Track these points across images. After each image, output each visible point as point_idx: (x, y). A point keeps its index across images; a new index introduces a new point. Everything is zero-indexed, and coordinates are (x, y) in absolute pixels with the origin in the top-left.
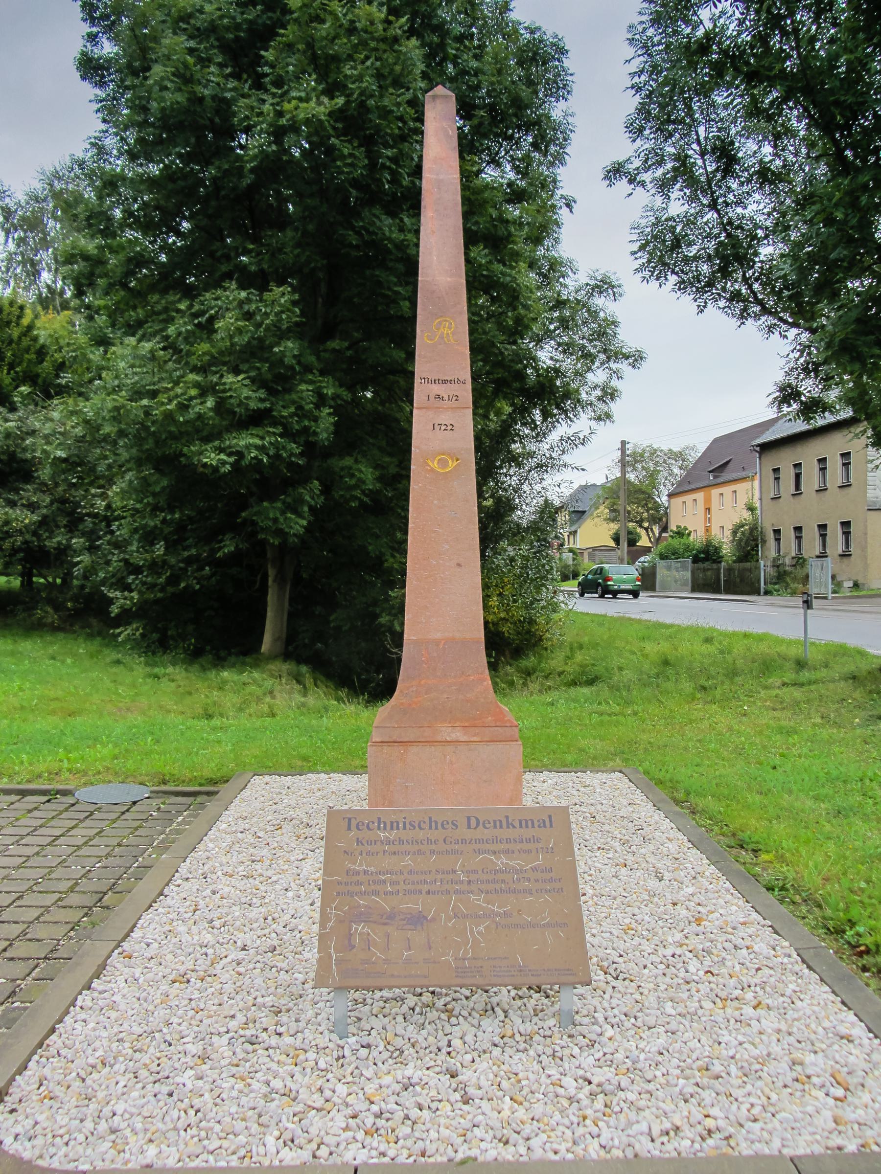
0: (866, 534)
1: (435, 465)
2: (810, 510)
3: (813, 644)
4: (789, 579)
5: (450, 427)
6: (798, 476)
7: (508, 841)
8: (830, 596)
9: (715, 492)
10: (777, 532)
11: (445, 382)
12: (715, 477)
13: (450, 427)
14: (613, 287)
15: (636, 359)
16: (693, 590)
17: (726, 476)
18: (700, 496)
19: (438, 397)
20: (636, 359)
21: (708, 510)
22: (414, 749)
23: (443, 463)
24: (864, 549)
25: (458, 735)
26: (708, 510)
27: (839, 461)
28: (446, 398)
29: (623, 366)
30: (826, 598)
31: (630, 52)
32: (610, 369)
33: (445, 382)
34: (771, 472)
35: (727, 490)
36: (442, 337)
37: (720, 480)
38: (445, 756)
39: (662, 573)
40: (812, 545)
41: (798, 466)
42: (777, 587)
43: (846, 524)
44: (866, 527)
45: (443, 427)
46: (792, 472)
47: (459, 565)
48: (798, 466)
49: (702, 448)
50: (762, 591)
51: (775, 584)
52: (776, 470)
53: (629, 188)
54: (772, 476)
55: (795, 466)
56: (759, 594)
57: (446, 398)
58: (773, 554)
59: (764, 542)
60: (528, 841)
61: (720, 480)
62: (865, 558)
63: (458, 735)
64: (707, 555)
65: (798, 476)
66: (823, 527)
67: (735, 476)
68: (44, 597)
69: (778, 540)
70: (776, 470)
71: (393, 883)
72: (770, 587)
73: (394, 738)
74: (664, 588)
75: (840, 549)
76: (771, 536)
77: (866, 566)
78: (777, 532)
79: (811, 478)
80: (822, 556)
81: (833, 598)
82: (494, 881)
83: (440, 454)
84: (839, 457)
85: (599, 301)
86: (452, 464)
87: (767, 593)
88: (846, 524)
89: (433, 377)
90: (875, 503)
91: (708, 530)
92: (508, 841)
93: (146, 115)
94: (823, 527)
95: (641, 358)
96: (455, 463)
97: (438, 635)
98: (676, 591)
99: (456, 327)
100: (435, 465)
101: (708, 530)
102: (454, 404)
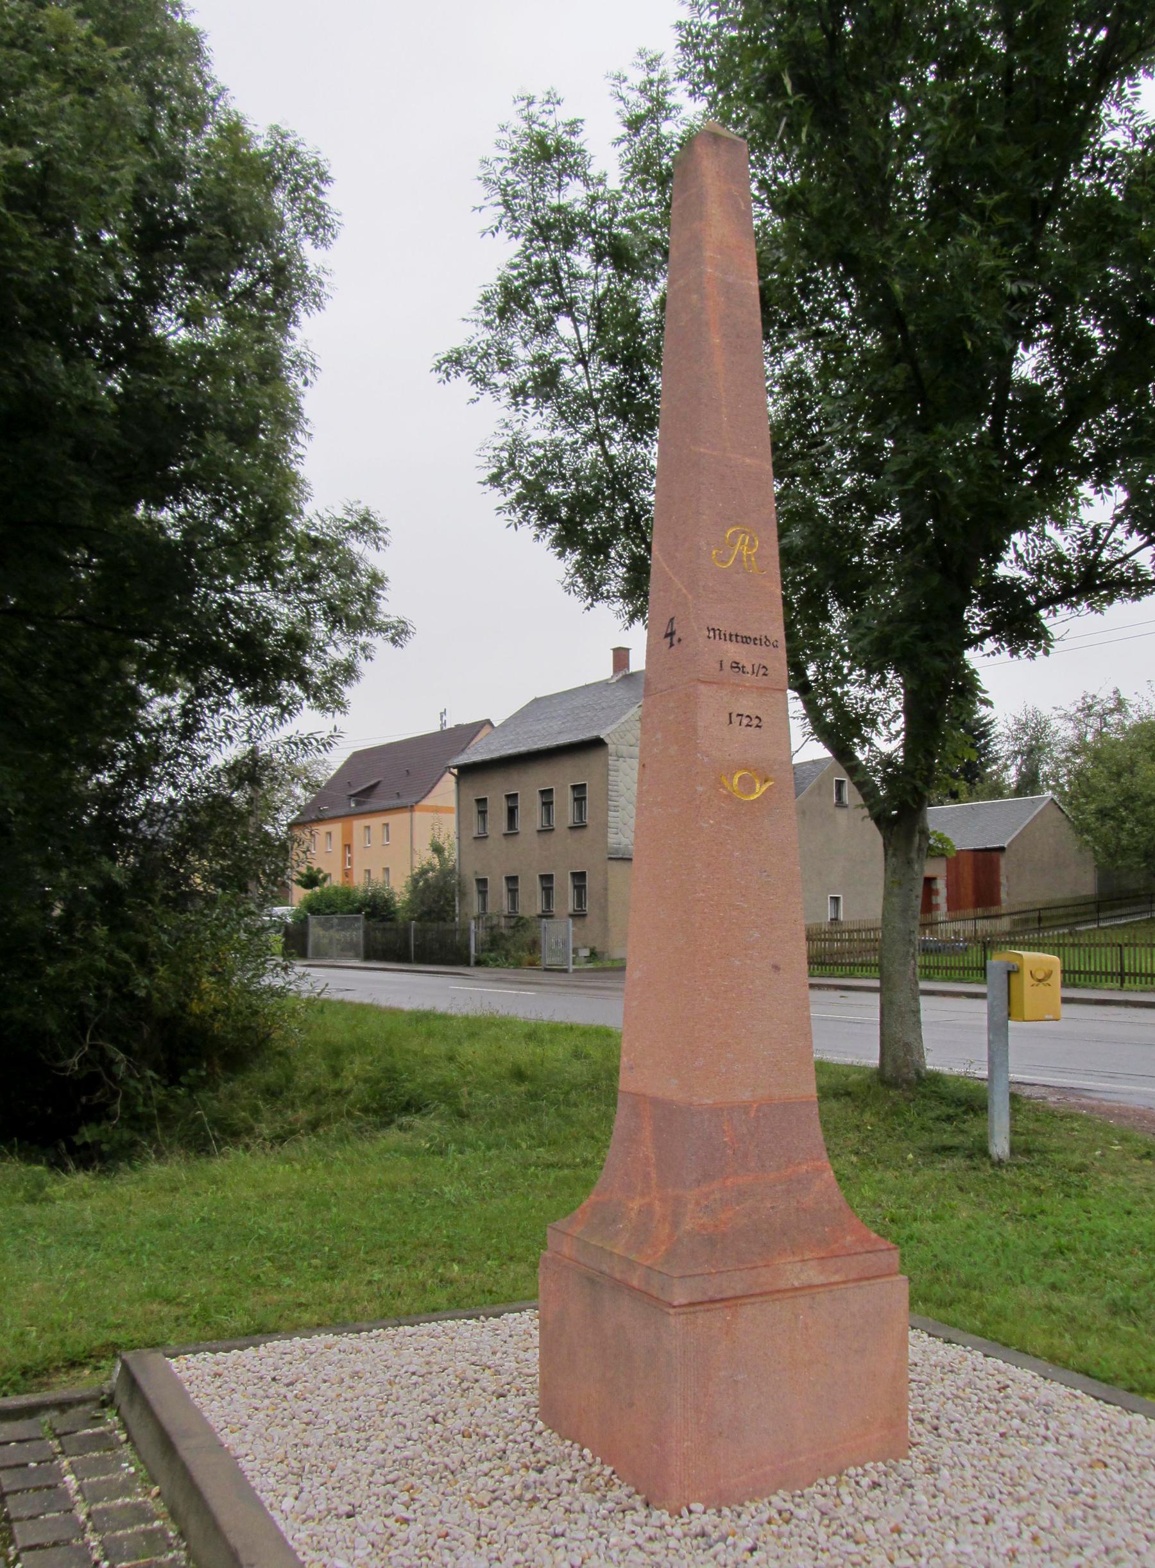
0: (606, 889)
2: (529, 855)
4: (510, 947)
5: (755, 722)
6: (512, 812)
8: (572, 967)
9: (358, 824)
10: (482, 882)
11: (746, 640)
12: (358, 803)
13: (755, 722)
14: (376, 529)
15: (398, 633)
16: (368, 957)
17: (374, 803)
18: (336, 828)
19: (736, 666)
20: (398, 633)
21: (348, 847)
22: (748, 1311)
24: (604, 908)
25: (812, 1275)
26: (348, 847)
27: (570, 795)
28: (749, 669)
29: (378, 642)
30: (566, 971)
31: (480, 193)
32: (356, 643)
33: (746, 640)
34: (474, 804)
35: (376, 822)
36: (739, 559)
37: (366, 808)
38: (797, 1316)
39: (316, 931)
40: (531, 904)
41: (512, 797)
42: (492, 955)
43: (579, 877)
44: (606, 881)
45: (745, 721)
46: (504, 805)
47: (776, 968)
48: (512, 797)
50: (472, 960)
51: (490, 951)
52: (481, 802)
53: (473, 390)
54: (475, 809)
55: (508, 797)
56: (468, 964)
57: (749, 669)
58: (476, 909)
59: (463, 894)
61: (366, 808)
62: (605, 920)
63: (812, 1275)
64: (376, 909)
65: (512, 812)
66: (547, 879)
67: (385, 803)
69: (483, 893)
70: (481, 802)
72: (484, 956)
73: (711, 1293)
74: (319, 954)
75: (571, 907)
76: (474, 888)
77: (606, 930)
78: (482, 882)
79: (531, 816)
80: (547, 915)
81: (575, 971)
84: (570, 791)
85: (356, 546)
86: (760, 789)
87: (479, 963)
88: (579, 877)
89: (726, 627)
90: (617, 851)
91: (347, 874)
94: (547, 879)
95: (407, 633)
96: (764, 788)
97: (746, 1096)
98: (340, 957)
99: (761, 547)
101: (347, 874)
102: (762, 681)
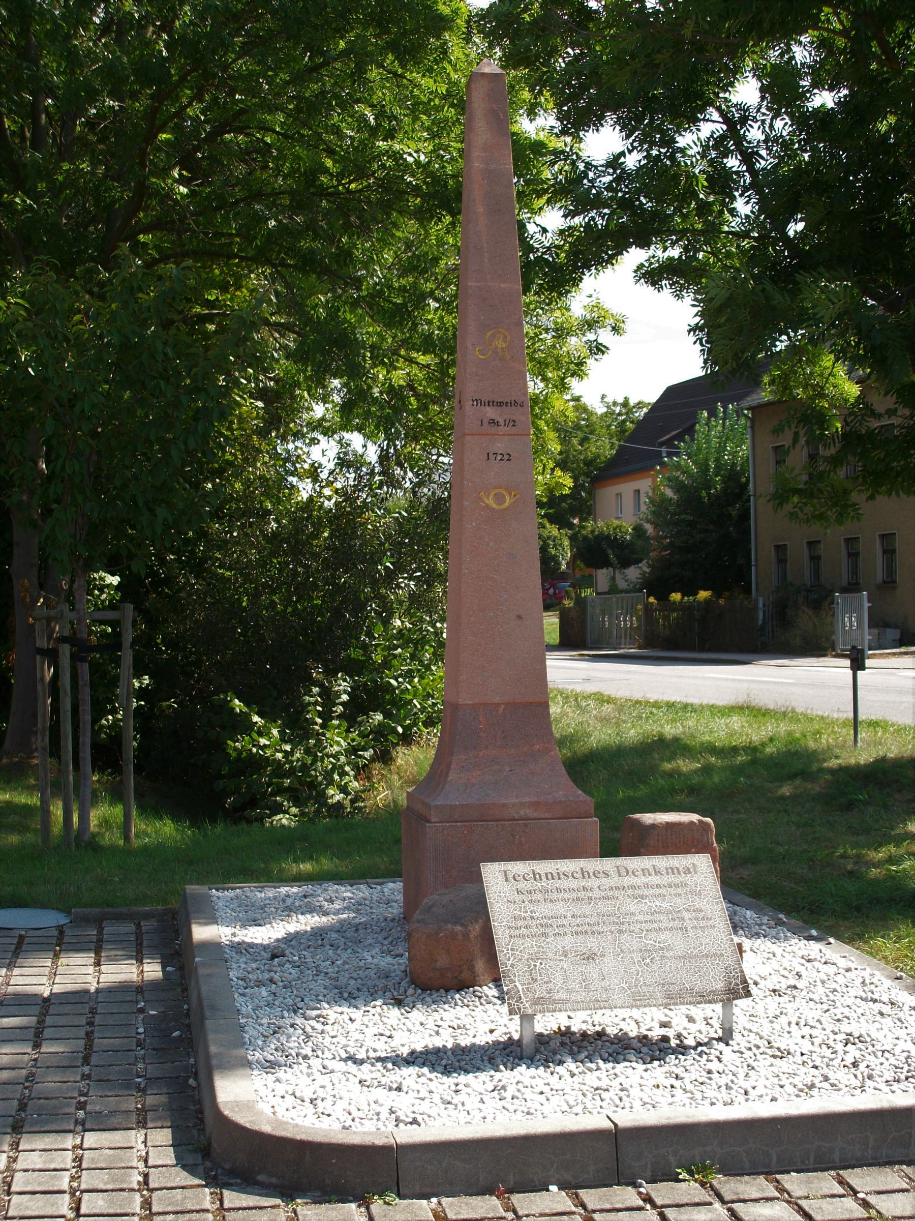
1: (491, 502)
3: (873, 724)
5: (506, 457)
7: (658, 886)
11: (500, 404)
13: (506, 457)
19: (493, 422)
23: (499, 499)
28: (502, 422)
33: (500, 404)
45: (499, 457)
49: (652, 396)
57: (502, 422)
60: (677, 886)
68: (21, 1114)
71: (526, 927)
82: (651, 922)
83: (495, 488)
92: (658, 886)
93: (353, 372)
100: (491, 502)
102: (509, 430)
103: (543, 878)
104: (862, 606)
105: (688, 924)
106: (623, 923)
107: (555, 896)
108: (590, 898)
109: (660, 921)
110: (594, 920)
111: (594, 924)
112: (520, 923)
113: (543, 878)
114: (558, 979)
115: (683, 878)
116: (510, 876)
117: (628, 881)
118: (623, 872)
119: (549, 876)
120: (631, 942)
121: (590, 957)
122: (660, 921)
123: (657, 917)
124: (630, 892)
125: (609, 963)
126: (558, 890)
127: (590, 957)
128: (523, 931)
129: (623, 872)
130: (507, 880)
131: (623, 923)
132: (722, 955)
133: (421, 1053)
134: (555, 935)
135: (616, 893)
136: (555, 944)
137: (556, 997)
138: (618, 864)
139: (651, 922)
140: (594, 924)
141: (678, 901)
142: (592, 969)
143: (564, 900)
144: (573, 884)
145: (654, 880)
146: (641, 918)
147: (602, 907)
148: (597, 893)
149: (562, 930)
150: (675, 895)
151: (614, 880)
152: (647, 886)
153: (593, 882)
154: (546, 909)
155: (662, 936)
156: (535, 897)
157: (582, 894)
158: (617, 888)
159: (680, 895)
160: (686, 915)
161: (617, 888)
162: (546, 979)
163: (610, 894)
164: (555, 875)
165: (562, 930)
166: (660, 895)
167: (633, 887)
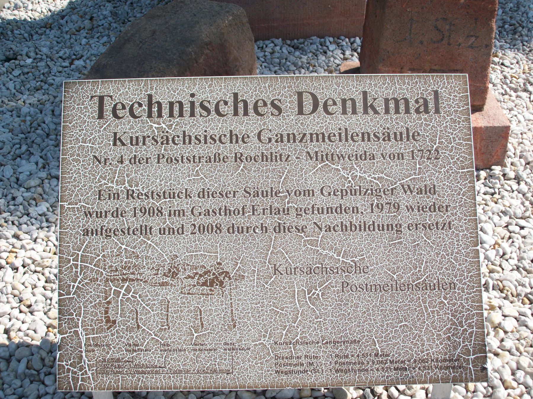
60: (399, 137)
82: (340, 210)
92: (366, 136)
103: (165, 111)
104: (118, 291)
105: (405, 218)
106: (286, 211)
107: (177, 150)
108: (238, 158)
109: (355, 210)
110: (238, 202)
111: (237, 212)
112: (109, 205)
113: (165, 111)
114: (152, 318)
115: (413, 121)
116: (108, 108)
117: (317, 122)
118: (308, 106)
119: (176, 109)
120: (294, 250)
121: (214, 280)
122: (355, 210)
123: (349, 201)
124: (313, 147)
125: (245, 294)
126: (186, 139)
127: (214, 280)
128: (110, 222)
129: (308, 106)
130: (101, 116)
131: (286, 211)
132: (452, 286)
133: (39, 348)
134: (162, 231)
135: (286, 148)
136: (160, 250)
137: (143, 359)
138: (303, 88)
139: (340, 210)
140: (237, 212)
141: (395, 168)
142: (214, 305)
143: (193, 159)
144: (216, 126)
145: (359, 122)
146: (320, 201)
147: (260, 176)
148: (253, 148)
149: (176, 222)
150: (392, 156)
151: (290, 122)
152: (346, 136)
153: (248, 125)
154: (156, 177)
155: (357, 239)
156: (142, 151)
157: (227, 149)
158: (291, 138)
159: (401, 156)
160: (405, 199)
161: (291, 138)
162: (131, 323)
163: (276, 148)
164: (187, 108)
165: (176, 222)
166: (364, 156)
167: (319, 137)
